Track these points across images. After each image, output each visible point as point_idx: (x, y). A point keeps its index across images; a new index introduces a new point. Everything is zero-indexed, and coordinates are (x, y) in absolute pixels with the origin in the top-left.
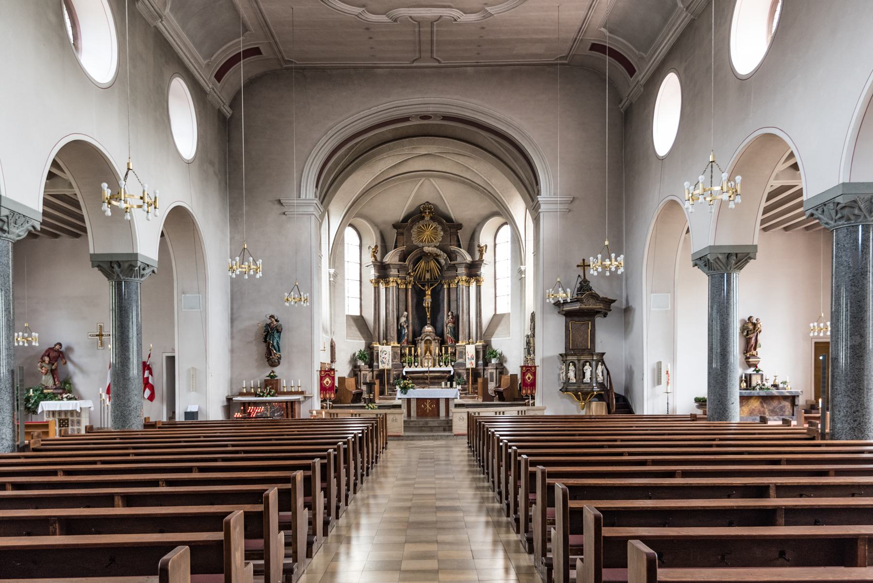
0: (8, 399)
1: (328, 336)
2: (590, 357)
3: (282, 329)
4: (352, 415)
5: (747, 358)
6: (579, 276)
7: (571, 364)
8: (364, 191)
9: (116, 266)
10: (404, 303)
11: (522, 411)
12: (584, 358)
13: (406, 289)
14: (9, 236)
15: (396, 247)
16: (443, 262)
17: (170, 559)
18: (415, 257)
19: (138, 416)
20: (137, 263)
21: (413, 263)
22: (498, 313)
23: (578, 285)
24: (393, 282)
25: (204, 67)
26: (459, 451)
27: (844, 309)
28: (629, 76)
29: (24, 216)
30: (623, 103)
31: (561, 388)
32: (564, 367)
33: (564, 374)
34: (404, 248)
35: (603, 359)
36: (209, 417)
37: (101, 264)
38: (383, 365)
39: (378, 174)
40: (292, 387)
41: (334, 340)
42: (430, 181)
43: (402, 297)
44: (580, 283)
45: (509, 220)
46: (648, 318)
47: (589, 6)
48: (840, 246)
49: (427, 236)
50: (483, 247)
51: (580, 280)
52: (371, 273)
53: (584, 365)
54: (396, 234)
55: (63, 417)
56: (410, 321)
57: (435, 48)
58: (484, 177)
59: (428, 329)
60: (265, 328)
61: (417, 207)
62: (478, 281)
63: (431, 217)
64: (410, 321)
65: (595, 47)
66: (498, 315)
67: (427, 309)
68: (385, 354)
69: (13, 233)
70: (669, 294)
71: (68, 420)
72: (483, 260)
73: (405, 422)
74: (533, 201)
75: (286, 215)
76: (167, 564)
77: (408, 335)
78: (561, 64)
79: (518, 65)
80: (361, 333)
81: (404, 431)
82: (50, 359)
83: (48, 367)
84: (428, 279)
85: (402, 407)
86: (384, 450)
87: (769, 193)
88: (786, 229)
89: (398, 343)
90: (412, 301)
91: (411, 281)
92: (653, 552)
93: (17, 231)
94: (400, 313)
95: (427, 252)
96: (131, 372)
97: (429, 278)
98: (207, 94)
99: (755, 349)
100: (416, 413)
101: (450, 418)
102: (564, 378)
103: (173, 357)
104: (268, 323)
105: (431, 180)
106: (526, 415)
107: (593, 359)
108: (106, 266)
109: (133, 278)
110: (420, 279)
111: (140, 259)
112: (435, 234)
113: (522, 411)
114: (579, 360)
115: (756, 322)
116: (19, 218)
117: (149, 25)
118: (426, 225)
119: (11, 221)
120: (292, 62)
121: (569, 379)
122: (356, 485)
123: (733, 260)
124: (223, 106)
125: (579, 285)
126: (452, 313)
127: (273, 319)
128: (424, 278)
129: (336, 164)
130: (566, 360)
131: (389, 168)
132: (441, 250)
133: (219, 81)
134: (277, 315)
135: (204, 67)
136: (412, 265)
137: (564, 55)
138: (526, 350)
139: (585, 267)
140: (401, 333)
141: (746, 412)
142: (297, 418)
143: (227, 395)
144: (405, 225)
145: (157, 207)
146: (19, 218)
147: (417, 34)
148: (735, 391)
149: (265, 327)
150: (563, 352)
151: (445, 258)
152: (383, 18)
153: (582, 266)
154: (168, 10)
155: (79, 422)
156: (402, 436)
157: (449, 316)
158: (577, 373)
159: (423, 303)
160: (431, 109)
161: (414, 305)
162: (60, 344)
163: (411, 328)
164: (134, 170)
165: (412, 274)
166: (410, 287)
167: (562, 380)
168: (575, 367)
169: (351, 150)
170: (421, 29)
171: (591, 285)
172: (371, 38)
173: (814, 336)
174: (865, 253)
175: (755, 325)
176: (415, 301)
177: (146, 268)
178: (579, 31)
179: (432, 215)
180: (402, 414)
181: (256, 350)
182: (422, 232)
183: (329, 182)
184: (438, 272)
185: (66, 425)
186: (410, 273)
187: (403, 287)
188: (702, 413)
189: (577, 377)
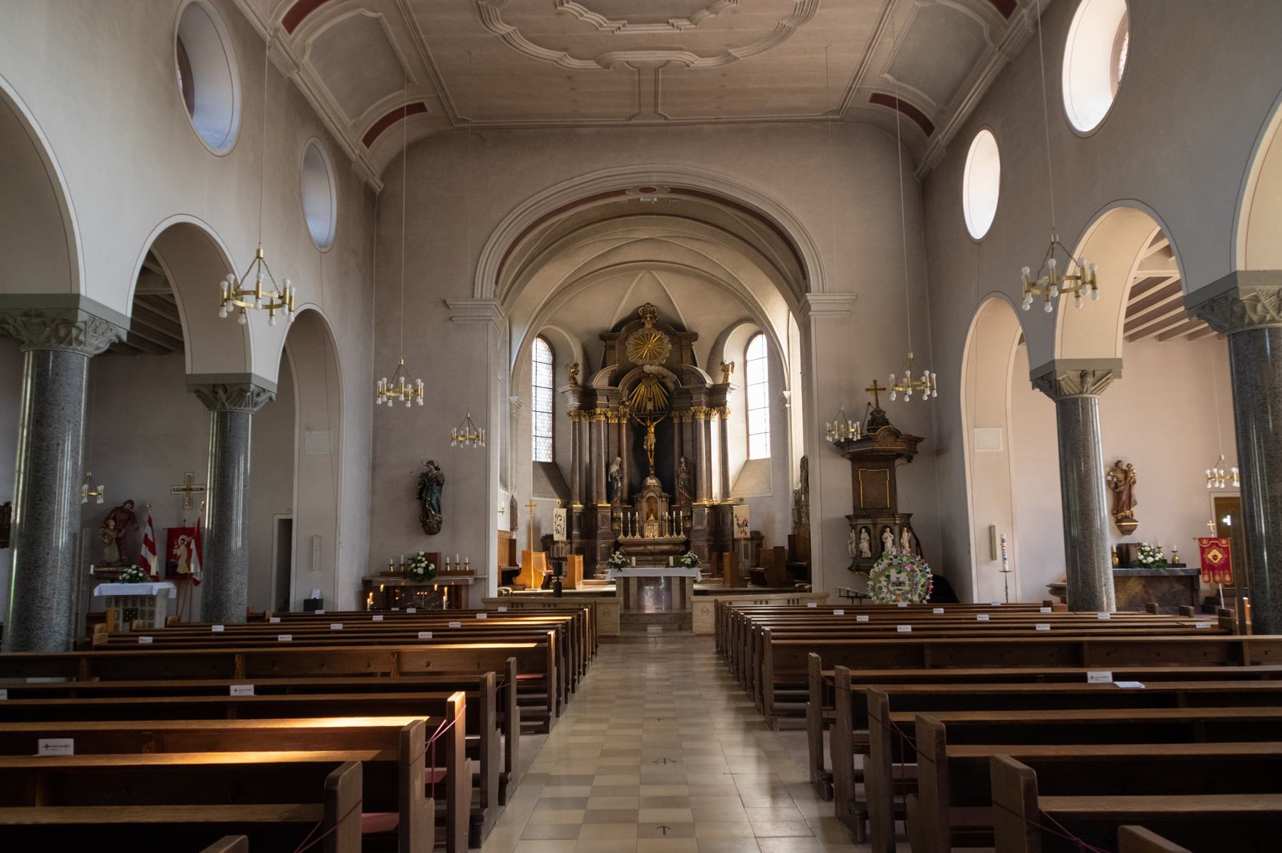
0: (67, 575)
1: (508, 491)
2: (891, 520)
3: (444, 481)
4: (544, 605)
5: (1118, 521)
6: (869, 404)
7: (863, 530)
8: (561, 289)
9: (221, 392)
10: (616, 444)
11: (793, 600)
12: (882, 521)
13: (619, 425)
14: (85, 349)
15: (604, 366)
16: (671, 386)
17: (340, 776)
18: (631, 380)
19: (240, 604)
20: (250, 386)
21: (629, 388)
22: (752, 458)
23: (869, 417)
24: (600, 414)
25: (349, 128)
26: (705, 661)
27: (1256, 445)
28: (925, 134)
29: (107, 322)
30: (919, 169)
31: (849, 566)
32: (853, 535)
33: (854, 545)
34: (615, 367)
35: (909, 523)
36: (338, 607)
37: (202, 389)
39: (581, 265)
40: (466, 564)
41: (515, 497)
42: (653, 275)
43: (614, 436)
44: (871, 414)
45: (764, 327)
46: (972, 461)
47: (867, 47)
48: (1240, 357)
49: (649, 350)
51: (871, 410)
52: (573, 402)
53: (883, 532)
54: (604, 348)
55: (130, 606)
56: (625, 471)
57: (660, 101)
58: (728, 270)
59: (652, 481)
60: (419, 479)
61: (635, 310)
62: (723, 414)
64: (625, 471)
65: (876, 98)
67: (649, 453)
69: (91, 345)
70: (1000, 430)
71: (136, 610)
72: (729, 384)
73: (621, 616)
74: (799, 302)
75: (454, 321)
76: (336, 783)
77: (622, 490)
78: (833, 120)
79: (772, 121)
80: (554, 486)
81: (621, 630)
82: (116, 523)
83: (114, 535)
84: (650, 410)
85: (617, 595)
86: (594, 656)
87: (1133, 288)
88: (1161, 337)
89: (608, 502)
90: (627, 441)
91: (626, 413)
92: (1029, 768)
93: (96, 342)
94: (610, 458)
95: (649, 372)
96: (234, 541)
97: (652, 408)
98: (352, 162)
99: (1129, 508)
101: (687, 611)
102: (854, 551)
103: (290, 521)
104: (424, 472)
105: (653, 272)
106: (800, 605)
107: (895, 524)
108: (207, 391)
109: (242, 408)
110: (639, 410)
111: (254, 381)
112: (659, 348)
113: (793, 600)
114: (875, 525)
115: (1127, 469)
116: (100, 325)
117: (282, 77)
118: (647, 335)
119: (90, 330)
120: (468, 121)
121: (861, 552)
122: (560, 704)
123: (1090, 380)
124: (372, 178)
125: (870, 416)
126: (686, 459)
127: (431, 466)
128: (645, 410)
129: (523, 253)
130: (856, 525)
131: (594, 258)
132: (668, 369)
133: (368, 146)
134: (438, 460)
135: (349, 128)
136: (627, 391)
137: (836, 108)
138: (795, 511)
139: (878, 391)
140: (613, 488)
141: (1123, 600)
142: (463, 608)
143: (362, 574)
144: (612, 338)
145: (292, 309)
146: (100, 325)
147: (636, 83)
148: (1107, 568)
149: (420, 477)
150: (851, 513)
152: (591, 64)
153: (876, 392)
154: (306, 58)
155: (152, 614)
156: (618, 637)
157: (681, 463)
158: (873, 542)
159: (643, 446)
160: (655, 179)
161: (631, 448)
162: (131, 502)
163: (625, 481)
164: (265, 259)
165: (627, 403)
166: (625, 422)
167: (851, 553)
168: (869, 535)
169: (544, 233)
170: (641, 77)
171: (887, 416)
172: (573, 89)
173: (1219, 487)
174: (1278, 366)
175: (1126, 473)
176: (632, 440)
177: (262, 394)
178: (855, 78)
179: (655, 321)
180: (617, 603)
181: (410, 509)
182: (640, 344)
183: (512, 277)
184: (664, 401)
185: (127, 619)
188: (1059, 601)
189: (874, 550)
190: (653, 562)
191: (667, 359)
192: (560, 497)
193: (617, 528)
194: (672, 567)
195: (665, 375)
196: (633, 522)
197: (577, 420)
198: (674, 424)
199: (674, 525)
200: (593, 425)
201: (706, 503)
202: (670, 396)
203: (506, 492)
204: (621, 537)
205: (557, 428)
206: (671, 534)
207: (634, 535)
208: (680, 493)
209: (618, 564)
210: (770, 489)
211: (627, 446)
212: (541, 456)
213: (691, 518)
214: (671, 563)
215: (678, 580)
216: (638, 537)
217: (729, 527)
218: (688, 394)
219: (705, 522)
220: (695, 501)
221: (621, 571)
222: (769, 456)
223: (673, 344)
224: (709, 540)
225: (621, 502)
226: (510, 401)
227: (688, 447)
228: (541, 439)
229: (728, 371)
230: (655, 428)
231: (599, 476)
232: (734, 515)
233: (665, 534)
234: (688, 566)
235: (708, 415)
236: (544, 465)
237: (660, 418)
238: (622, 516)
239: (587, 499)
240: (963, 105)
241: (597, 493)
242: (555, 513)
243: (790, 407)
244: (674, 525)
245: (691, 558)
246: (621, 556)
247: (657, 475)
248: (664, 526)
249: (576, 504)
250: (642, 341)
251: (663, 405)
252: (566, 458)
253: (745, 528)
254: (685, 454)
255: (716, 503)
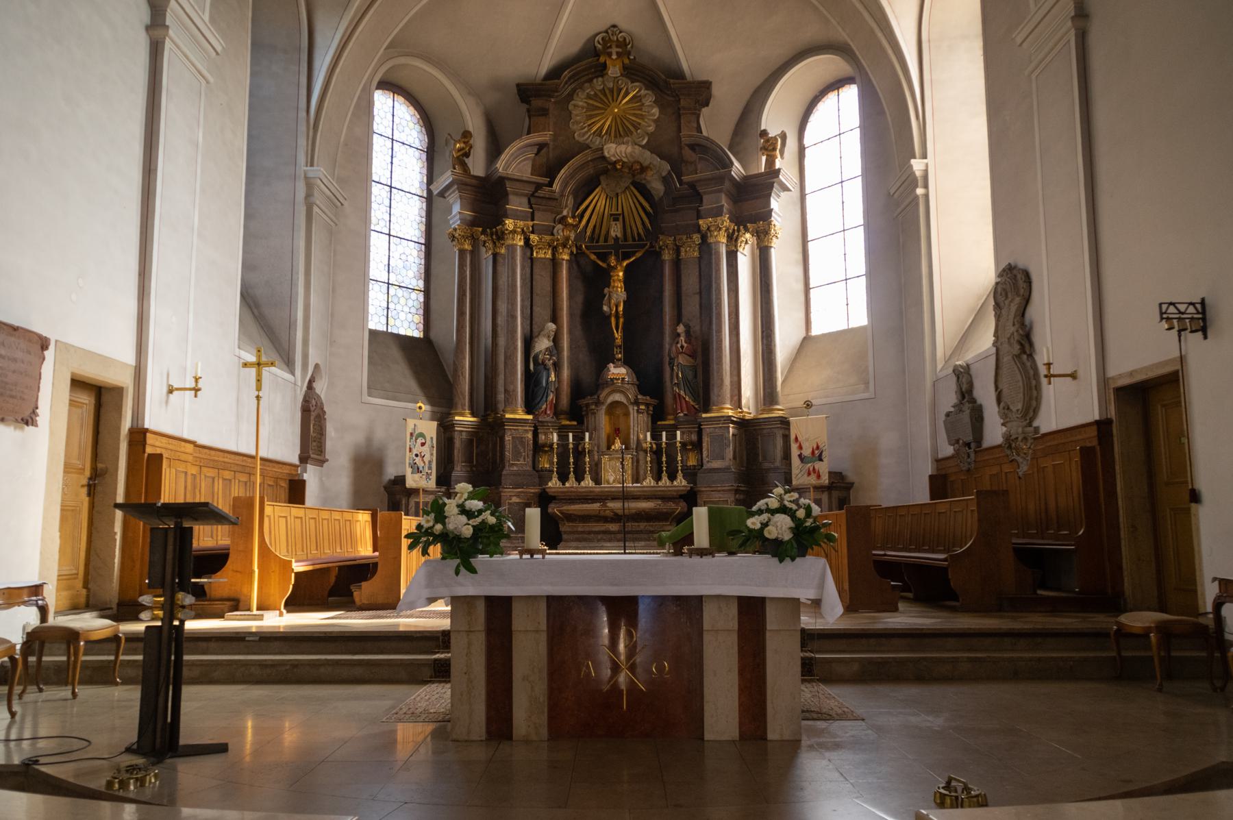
1: (293, 374)
10: (548, 299)
13: (555, 263)
16: (657, 187)
18: (578, 177)
21: (575, 193)
22: (816, 331)
24: (514, 232)
38: (417, 476)
49: (615, 119)
50: (775, 138)
56: (565, 353)
59: (617, 371)
63: (625, 68)
64: (565, 353)
66: (817, 337)
67: (613, 320)
68: (423, 444)
84: (616, 239)
89: (528, 413)
90: (571, 297)
94: (535, 326)
100: (544, 718)
128: (606, 241)
140: (538, 383)
151: (664, 174)
157: (679, 335)
163: (566, 373)
165: (570, 221)
166: (566, 257)
176: (580, 298)
179: (627, 61)
182: (600, 108)
184: (643, 223)
186: (564, 218)
187: (544, 254)
190: (620, 536)
191: (650, 135)
192: (431, 400)
193: (547, 466)
194: (702, 553)
195: (646, 164)
196: (579, 453)
197: (467, 247)
198: (663, 262)
199: (664, 459)
200: (500, 259)
201: (730, 413)
202: (656, 210)
203: (288, 376)
204: (554, 484)
205: (434, 271)
206: (658, 478)
207: (579, 478)
208: (676, 397)
209: (458, 538)
210: (867, 383)
211: (570, 307)
212: (398, 323)
213: (698, 446)
214: (702, 537)
215: (734, 610)
216: (588, 482)
217: (778, 464)
218: (694, 195)
219: (729, 452)
220: (707, 411)
221: (472, 570)
222: (860, 318)
223: (662, 108)
224: (737, 491)
225: (557, 413)
226: (306, 178)
227: (691, 307)
228: (400, 292)
229: (774, 149)
230: (627, 271)
231: (510, 358)
232: (793, 437)
233: (645, 479)
234: (777, 549)
235: (733, 239)
236: (405, 343)
237: (634, 254)
238: (555, 440)
239: (488, 409)
240: (582, 551)
241: (506, 391)
242: (409, 430)
243: (927, 196)
244: (664, 459)
245: (791, 513)
246: (477, 504)
247: (627, 362)
248: (641, 462)
249: (462, 415)
250: (602, 102)
251: (641, 231)
252: (447, 333)
253: (818, 465)
254: (684, 319)
255: (748, 417)
